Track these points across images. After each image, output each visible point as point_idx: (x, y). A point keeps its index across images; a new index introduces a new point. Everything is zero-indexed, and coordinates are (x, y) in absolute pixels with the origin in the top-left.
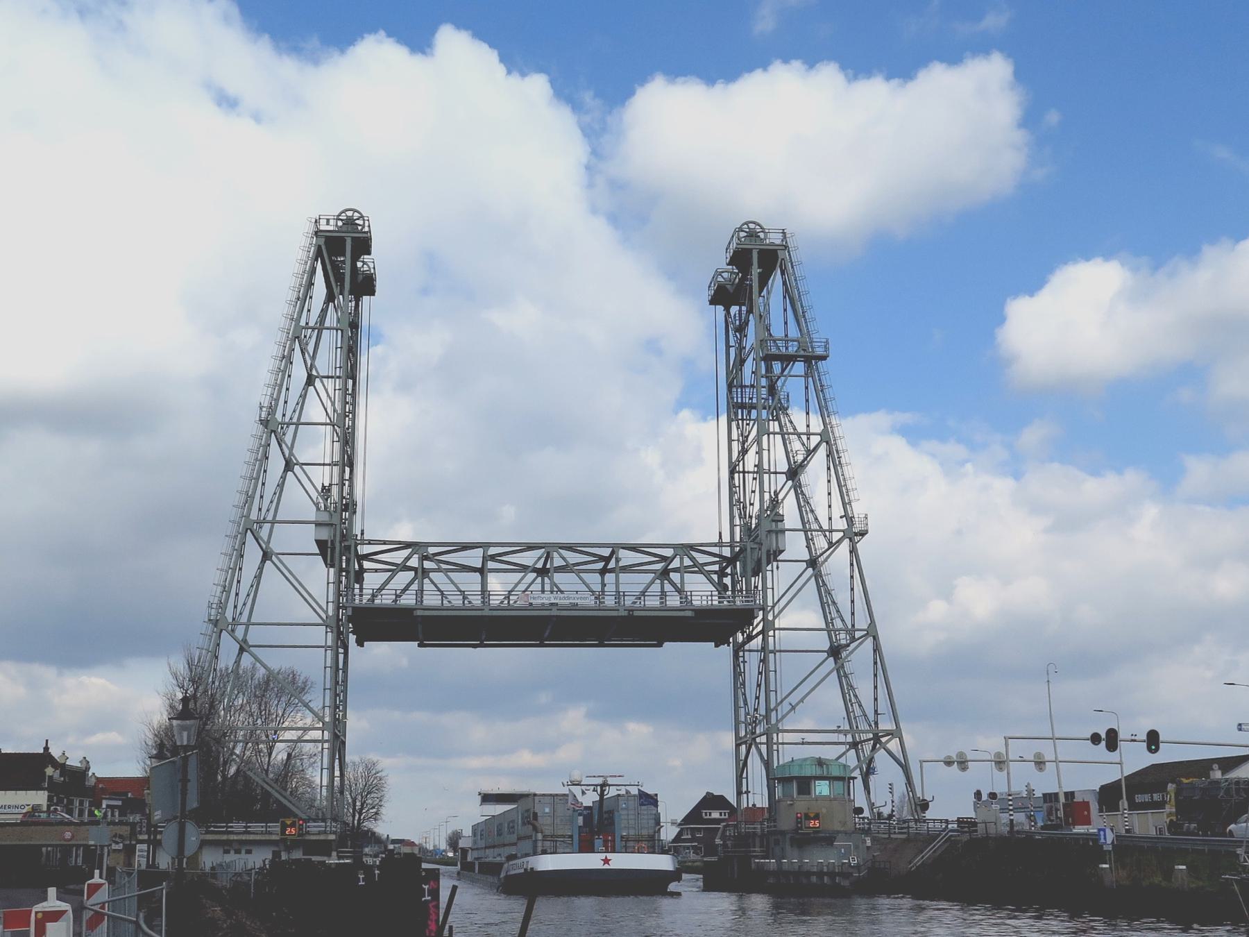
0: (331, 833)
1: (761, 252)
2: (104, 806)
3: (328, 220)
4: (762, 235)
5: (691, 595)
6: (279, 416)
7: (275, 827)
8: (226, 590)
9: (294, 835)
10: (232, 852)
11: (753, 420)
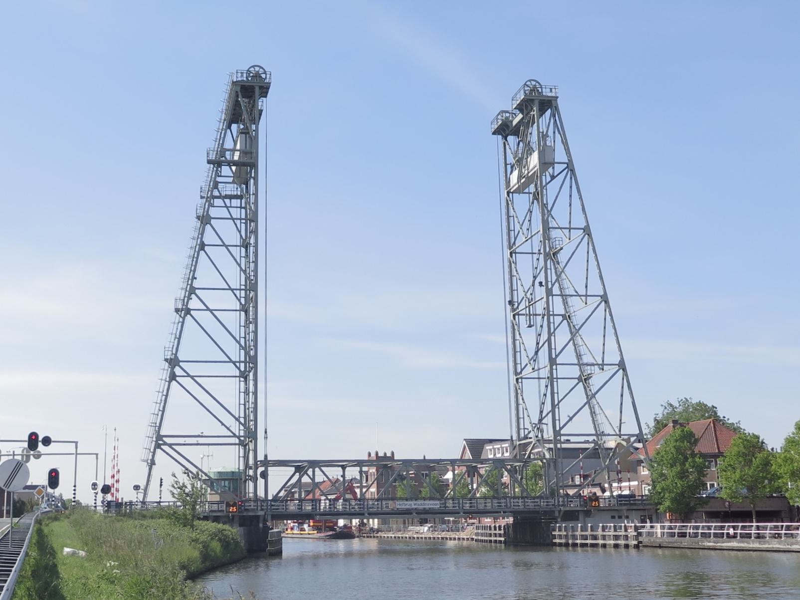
3: (551, 89)
4: (263, 76)
5: (168, 350)
9: (236, 512)
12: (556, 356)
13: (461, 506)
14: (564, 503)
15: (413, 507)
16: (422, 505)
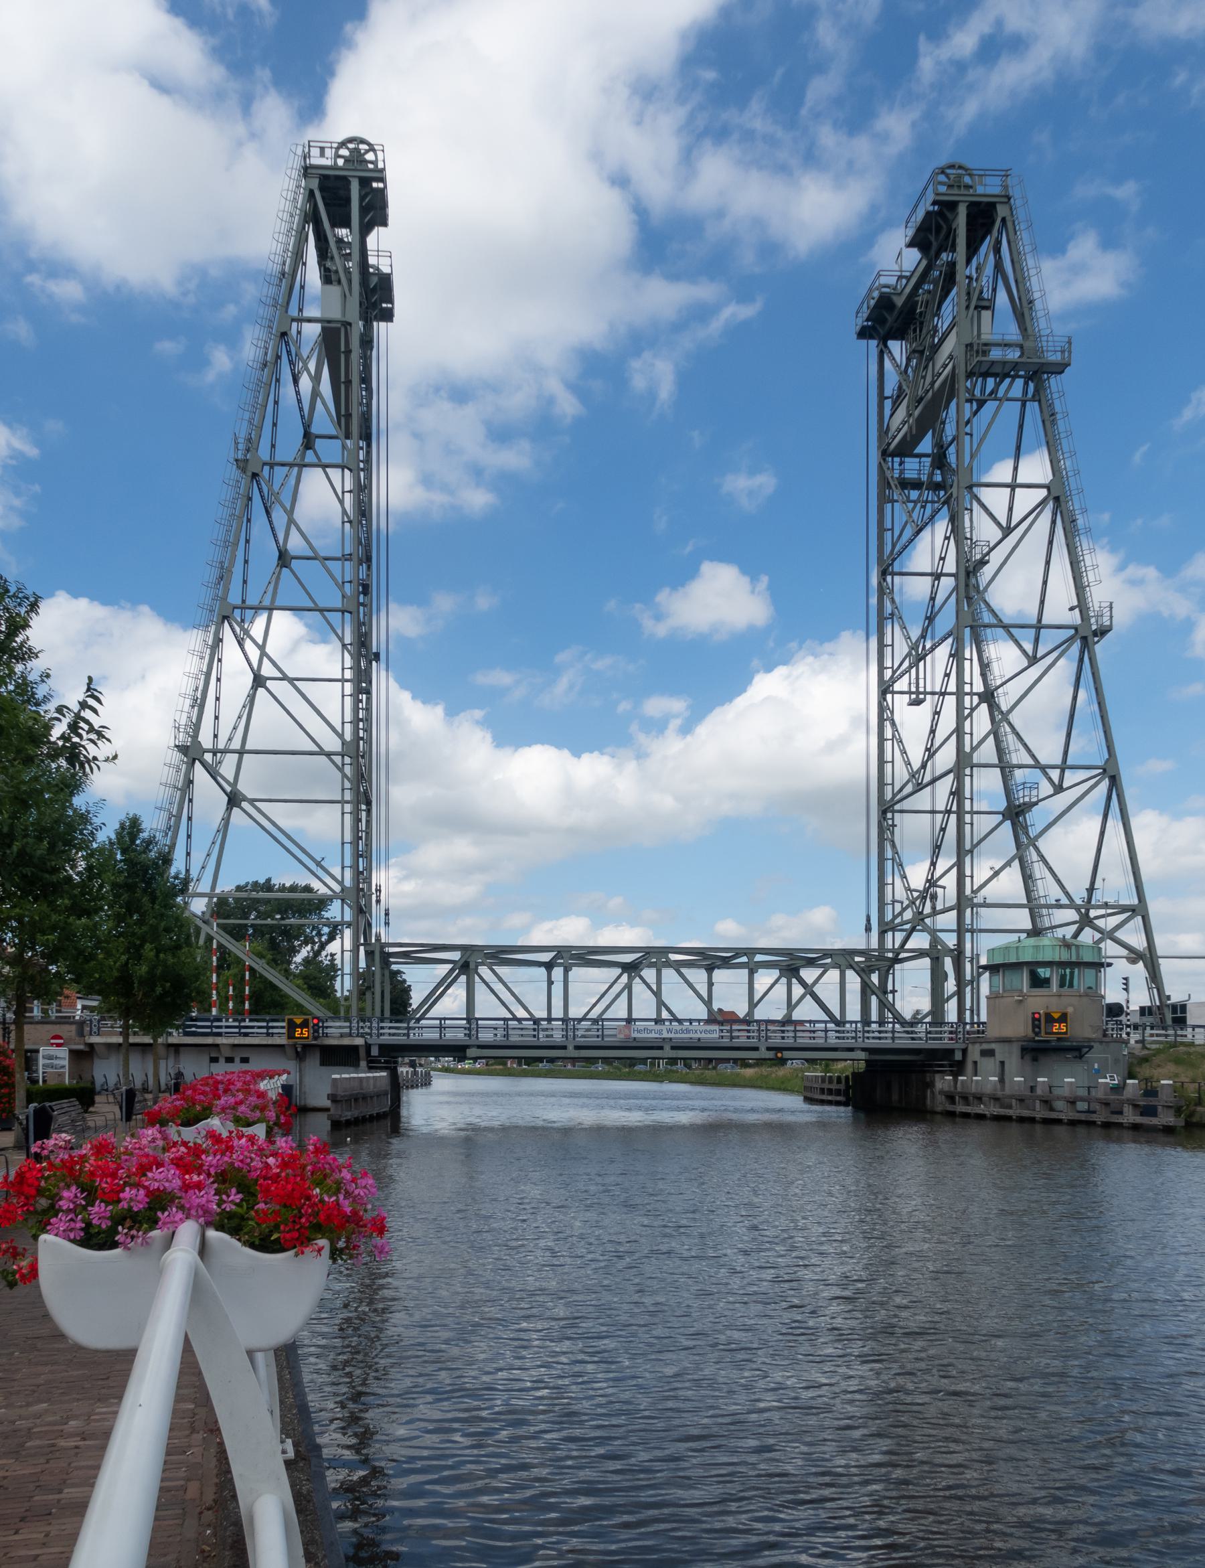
0: (357, 1036)
1: (972, 206)
2: (79, 1007)
3: (322, 149)
6: (264, 453)
7: (280, 1027)
8: (199, 704)
9: (307, 1038)
10: (222, 1060)
11: (912, 502)
12: (973, 892)
13: (570, 1033)
14: (351, 1030)
15: (665, 1035)
16: (683, 1032)
